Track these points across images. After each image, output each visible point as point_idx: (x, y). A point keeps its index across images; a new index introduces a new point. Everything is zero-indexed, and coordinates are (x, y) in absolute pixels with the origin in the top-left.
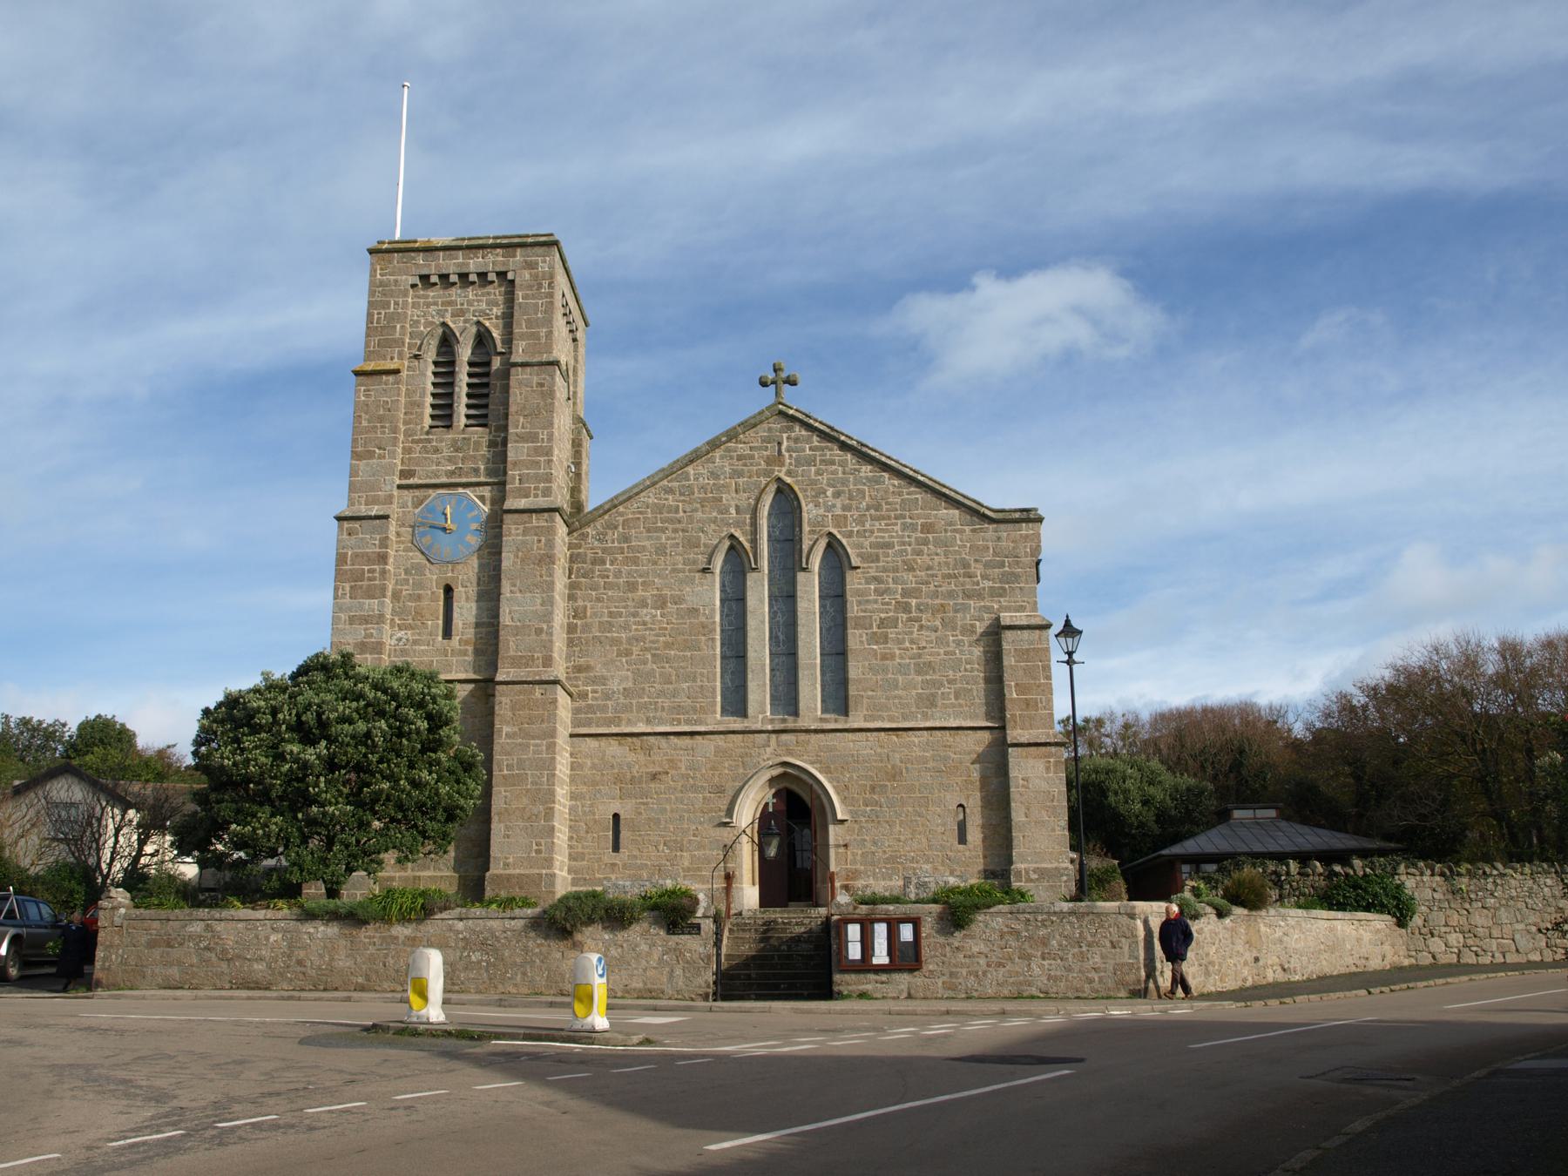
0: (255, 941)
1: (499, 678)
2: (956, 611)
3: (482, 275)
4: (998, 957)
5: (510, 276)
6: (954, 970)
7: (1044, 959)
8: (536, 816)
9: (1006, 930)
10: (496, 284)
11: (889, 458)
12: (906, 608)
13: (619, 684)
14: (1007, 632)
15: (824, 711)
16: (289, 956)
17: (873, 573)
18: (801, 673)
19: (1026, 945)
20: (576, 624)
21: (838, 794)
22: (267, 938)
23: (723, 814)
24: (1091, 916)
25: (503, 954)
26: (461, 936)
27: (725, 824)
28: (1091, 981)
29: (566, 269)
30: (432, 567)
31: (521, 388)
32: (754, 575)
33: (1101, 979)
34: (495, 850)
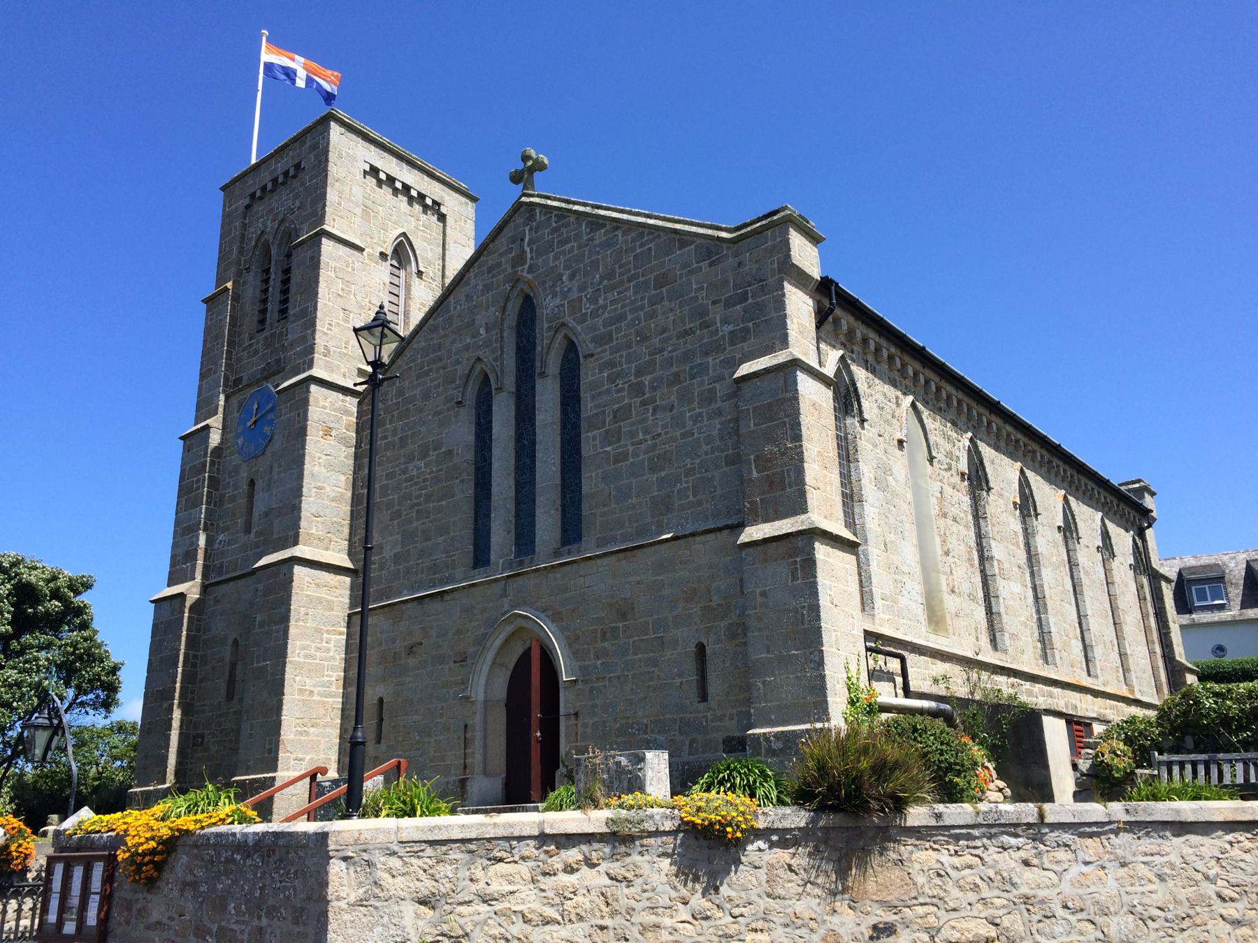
2: (692, 377)
12: (637, 389)
13: (391, 550)
17: (607, 356)
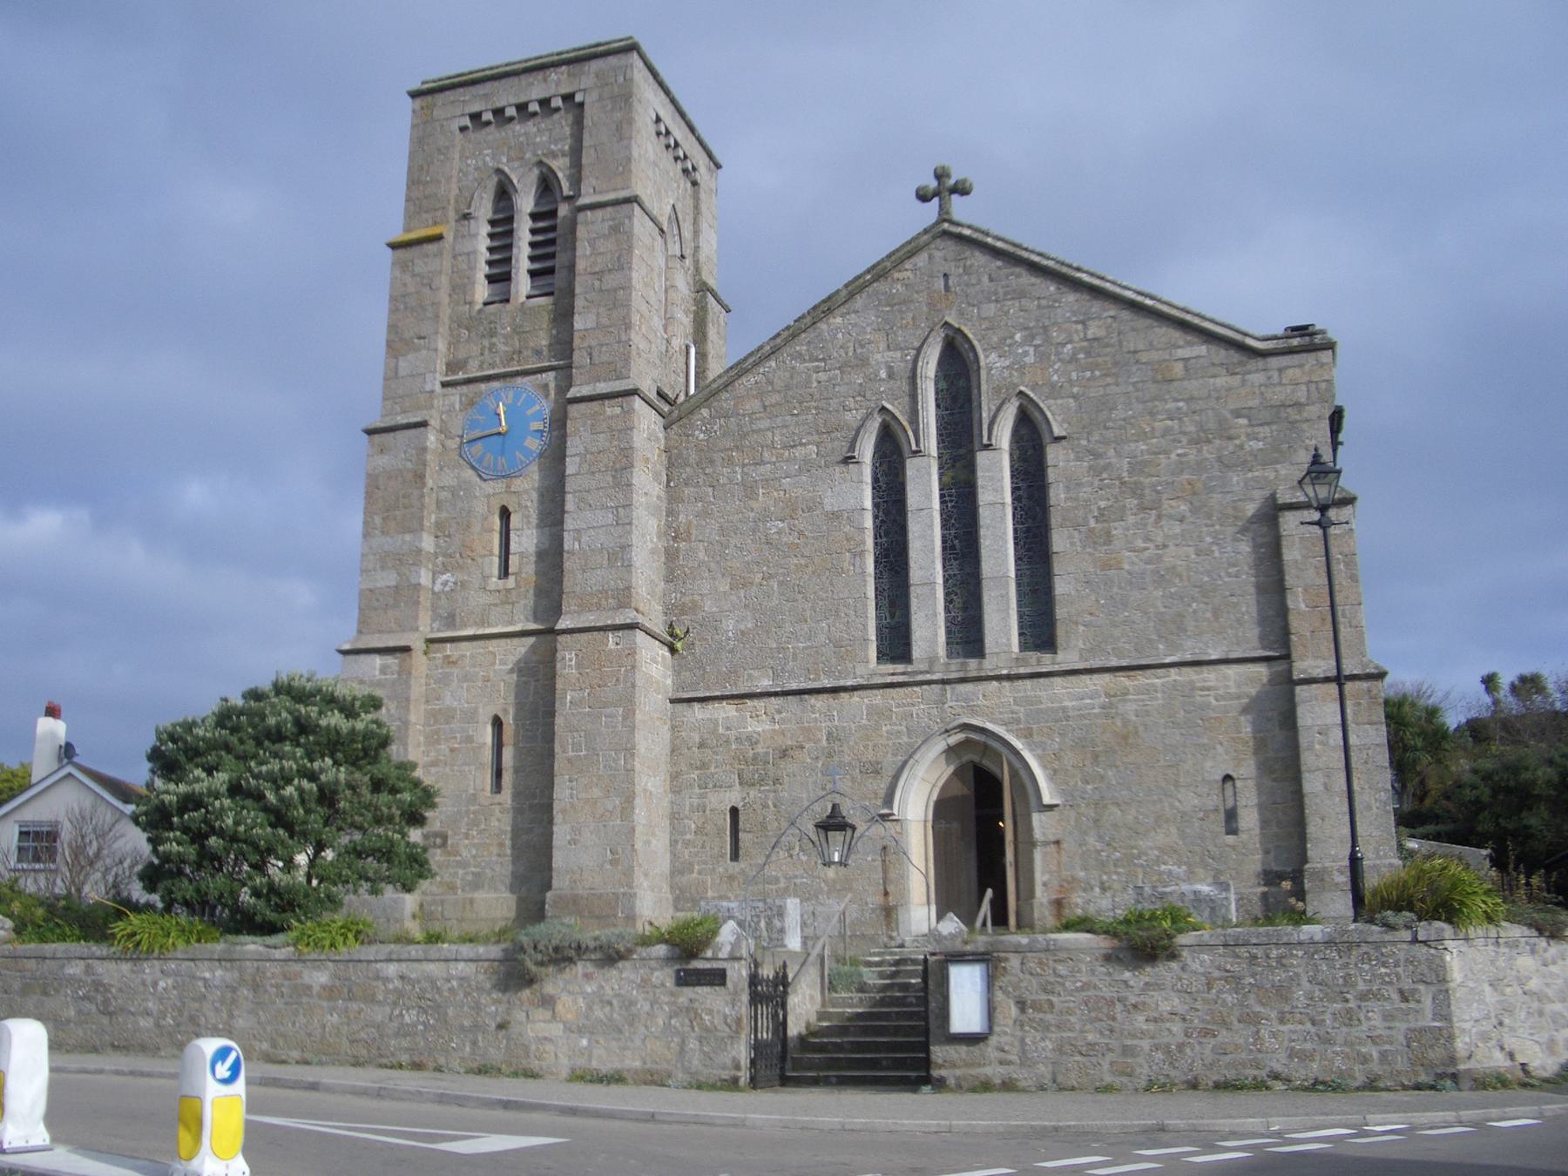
0: (141, 988)
1: (562, 624)
3: (545, 103)
4: (1203, 1021)
5: (578, 98)
6: (1129, 1042)
7: (1282, 1021)
8: (611, 812)
9: (1216, 974)
10: (562, 112)
11: (1102, 278)
14: (1287, 514)
15: (1024, 647)
16: (180, 1011)
18: (988, 596)
19: (1252, 1000)
20: (677, 549)
21: (1044, 767)
22: (155, 984)
23: (879, 802)
24: (1364, 948)
25: (446, 1013)
26: (391, 986)
27: (884, 817)
28: (1365, 1059)
29: (661, 84)
30: (483, 485)
31: (590, 232)
32: (917, 461)
33: (1383, 1055)
34: (558, 860)
